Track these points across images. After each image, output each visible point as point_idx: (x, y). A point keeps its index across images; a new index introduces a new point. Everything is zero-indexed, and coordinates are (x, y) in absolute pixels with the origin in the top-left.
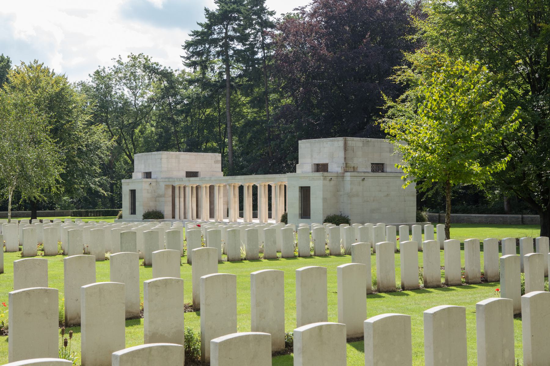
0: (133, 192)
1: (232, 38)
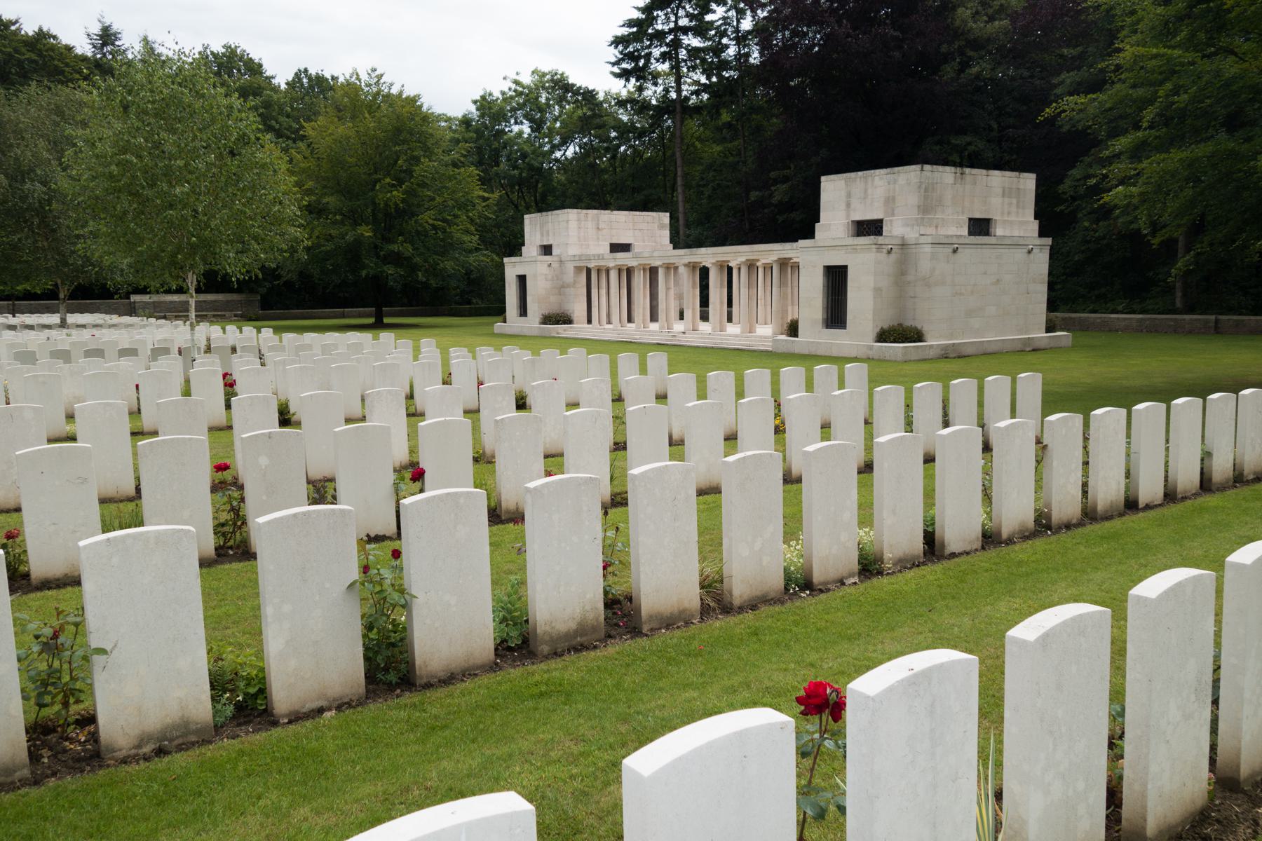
0: (522, 279)
1: (685, 30)
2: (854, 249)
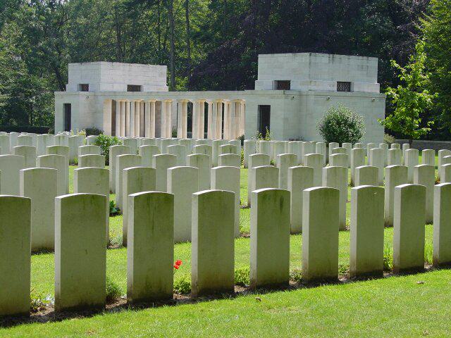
2: (273, 97)
